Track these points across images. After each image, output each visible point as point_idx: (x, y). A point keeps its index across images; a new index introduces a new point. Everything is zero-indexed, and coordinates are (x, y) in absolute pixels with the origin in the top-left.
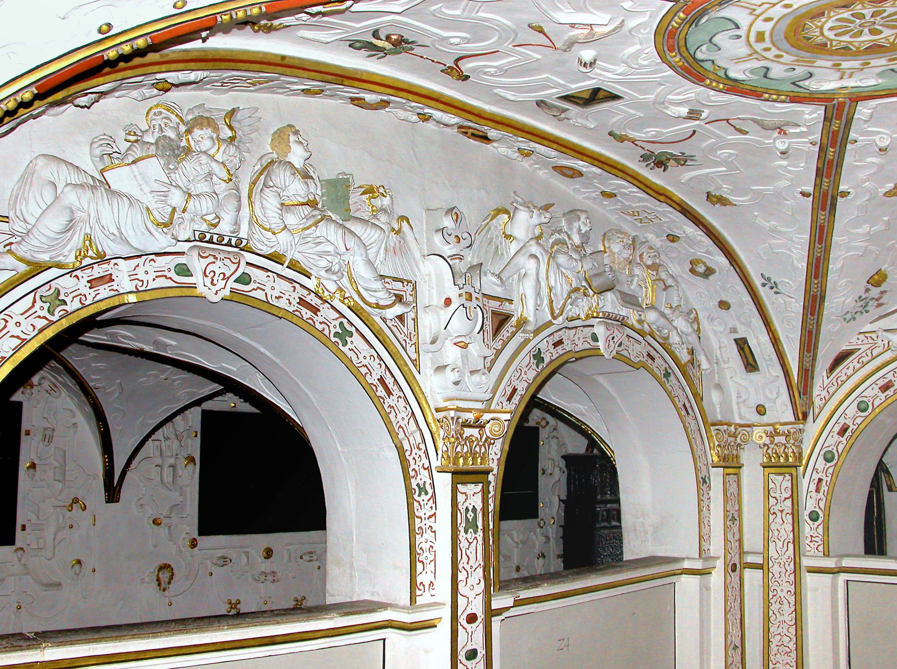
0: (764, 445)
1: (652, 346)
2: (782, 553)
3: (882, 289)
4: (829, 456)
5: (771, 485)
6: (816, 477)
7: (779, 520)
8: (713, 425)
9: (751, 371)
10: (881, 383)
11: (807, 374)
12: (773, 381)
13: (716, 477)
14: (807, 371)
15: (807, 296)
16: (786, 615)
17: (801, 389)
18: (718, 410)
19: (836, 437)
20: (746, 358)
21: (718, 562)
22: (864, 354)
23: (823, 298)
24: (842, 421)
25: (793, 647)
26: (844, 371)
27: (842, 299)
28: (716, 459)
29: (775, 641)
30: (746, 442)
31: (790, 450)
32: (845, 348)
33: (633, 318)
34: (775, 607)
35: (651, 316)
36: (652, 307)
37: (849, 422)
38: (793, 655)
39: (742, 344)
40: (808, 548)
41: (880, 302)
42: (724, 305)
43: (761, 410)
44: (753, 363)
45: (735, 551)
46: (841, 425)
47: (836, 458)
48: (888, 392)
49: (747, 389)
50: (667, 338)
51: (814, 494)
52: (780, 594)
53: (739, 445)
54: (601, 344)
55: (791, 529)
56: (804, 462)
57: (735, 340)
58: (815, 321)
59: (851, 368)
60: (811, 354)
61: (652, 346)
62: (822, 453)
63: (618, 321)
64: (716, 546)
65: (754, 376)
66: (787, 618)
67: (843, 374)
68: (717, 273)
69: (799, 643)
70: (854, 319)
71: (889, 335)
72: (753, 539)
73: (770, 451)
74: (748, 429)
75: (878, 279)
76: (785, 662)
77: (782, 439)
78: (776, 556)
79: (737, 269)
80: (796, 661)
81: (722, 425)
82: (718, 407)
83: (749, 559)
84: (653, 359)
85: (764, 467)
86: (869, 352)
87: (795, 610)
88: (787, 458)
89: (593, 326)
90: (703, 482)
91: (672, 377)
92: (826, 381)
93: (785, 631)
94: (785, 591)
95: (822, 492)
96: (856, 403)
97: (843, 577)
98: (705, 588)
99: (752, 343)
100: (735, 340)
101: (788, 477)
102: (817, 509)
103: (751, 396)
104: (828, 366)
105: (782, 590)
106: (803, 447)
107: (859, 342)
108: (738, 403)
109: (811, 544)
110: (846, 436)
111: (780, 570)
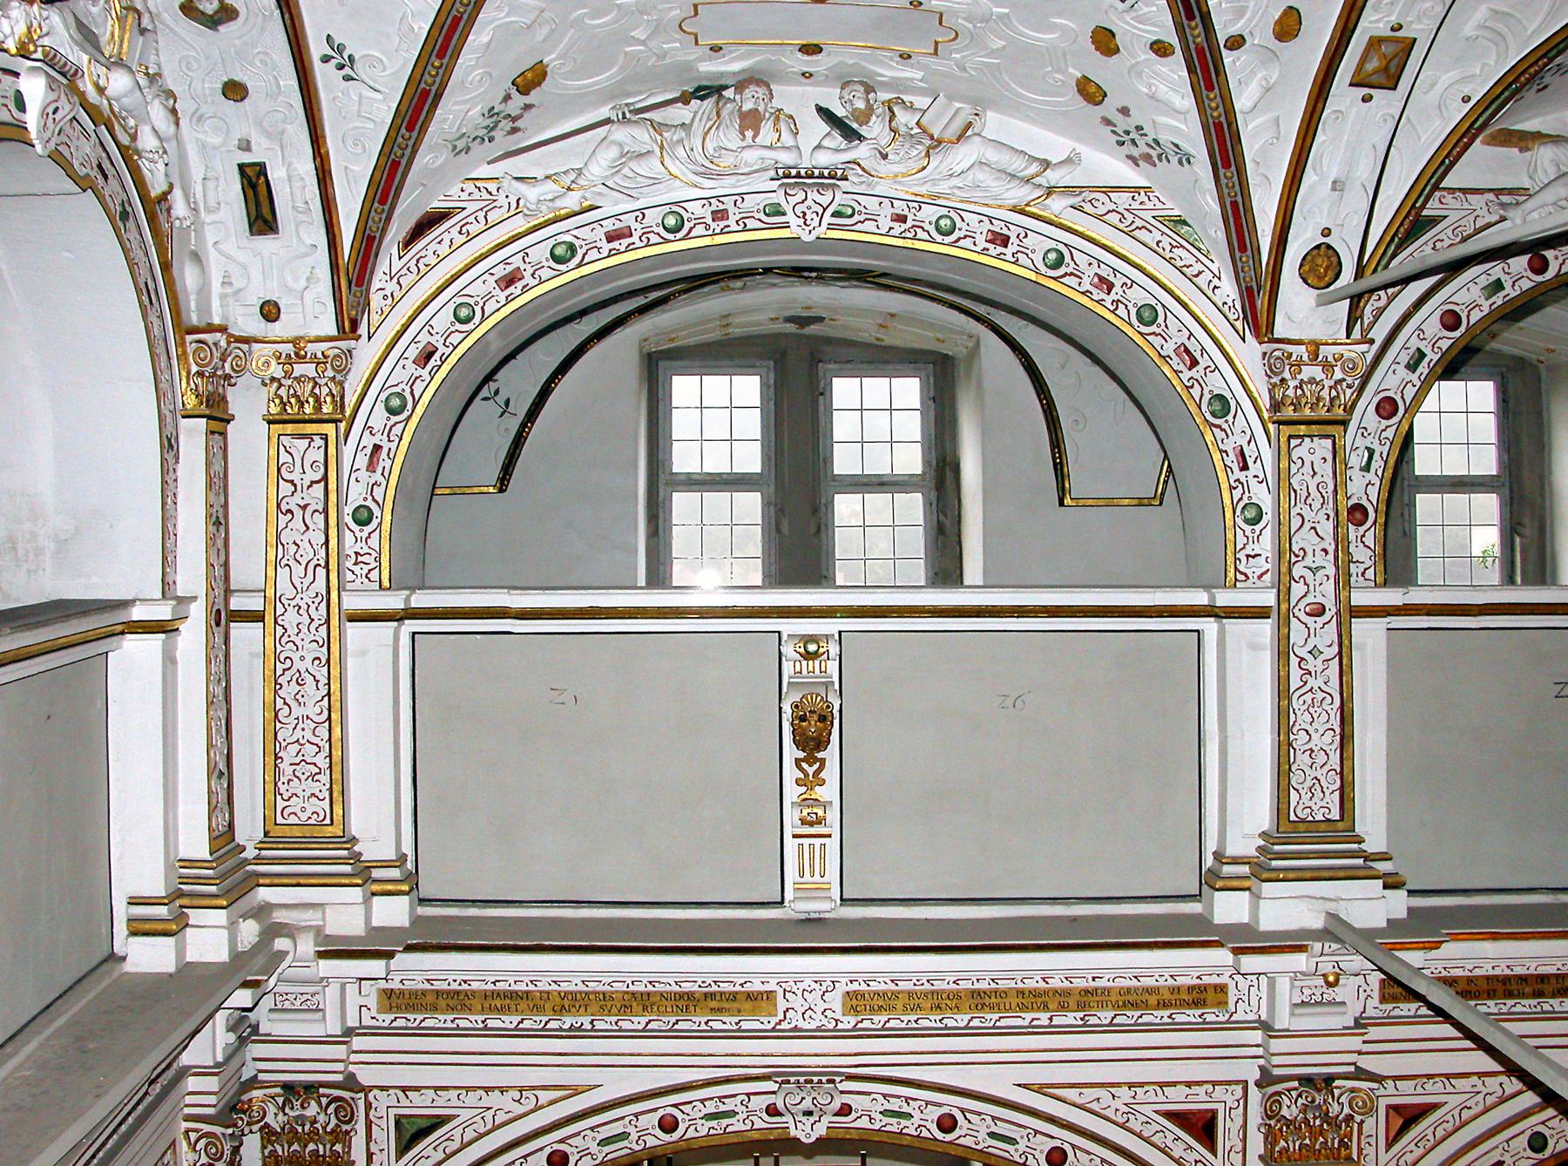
0: (273, 379)
1: (105, 150)
2: (299, 587)
3: (527, 100)
4: (396, 402)
5: (284, 457)
6: (369, 441)
7: (298, 523)
8: (190, 332)
9: (261, 233)
10: (500, 272)
11: (368, 245)
12: (305, 255)
13: (193, 434)
14: (371, 239)
15: (411, 92)
16: (310, 703)
17: (352, 277)
18: (193, 305)
19: (412, 368)
20: (258, 204)
21: (193, 606)
22: (471, 219)
23: (439, 96)
24: (424, 338)
25: (322, 762)
26: (434, 246)
27: (465, 107)
28: (191, 401)
29: (289, 755)
30: (239, 370)
31: (325, 390)
32: (436, 204)
33: (91, 74)
34: (288, 691)
35: (118, 82)
36: (119, 63)
37: (437, 341)
38: (325, 778)
39: (254, 181)
40: (350, 576)
41: (517, 124)
42: (235, 91)
43: (270, 312)
44: (269, 218)
45: (219, 591)
46: (421, 346)
47: (409, 406)
48: (511, 289)
49: (244, 267)
50: (134, 138)
51: (363, 474)
52: (298, 665)
53: (227, 377)
54: (32, 119)
55: (323, 540)
56: (348, 413)
57: (241, 167)
58: (411, 143)
59: (446, 243)
60: (386, 207)
61: (105, 150)
62: (383, 396)
63: (64, 75)
64: (192, 576)
65: (265, 243)
66: (312, 711)
67: (430, 253)
68: (240, 20)
69: (337, 754)
70: (468, 149)
71: (522, 188)
72: (248, 567)
73: (283, 392)
74: (245, 347)
75: (530, 80)
76: (308, 794)
77: (309, 370)
78: (291, 592)
79: (287, 16)
80: (331, 790)
81: (210, 332)
82: (193, 298)
83: (236, 603)
84: (106, 177)
85: (270, 422)
86: (481, 215)
87: (329, 694)
88: (318, 408)
89: (17, 75)
90: (169, 445)
91: (131, 224)
92: (397, 265)
93: (308, 735)
94: (309, 659)
95: (379, 471)
96: (451, 306)
97: (411, 625)
98: (169, 659)
99: (276, 175)
100: (241, 167)
101: (318, 442)
102: (370, 503)
103: (268, 280)
104: (402, 235)
105: (302, 658)
106: (346, 386)
107: (464, 196)
108: (223, 297)
109: (356, 569)
110: (429, 367)
111: (300, 619)
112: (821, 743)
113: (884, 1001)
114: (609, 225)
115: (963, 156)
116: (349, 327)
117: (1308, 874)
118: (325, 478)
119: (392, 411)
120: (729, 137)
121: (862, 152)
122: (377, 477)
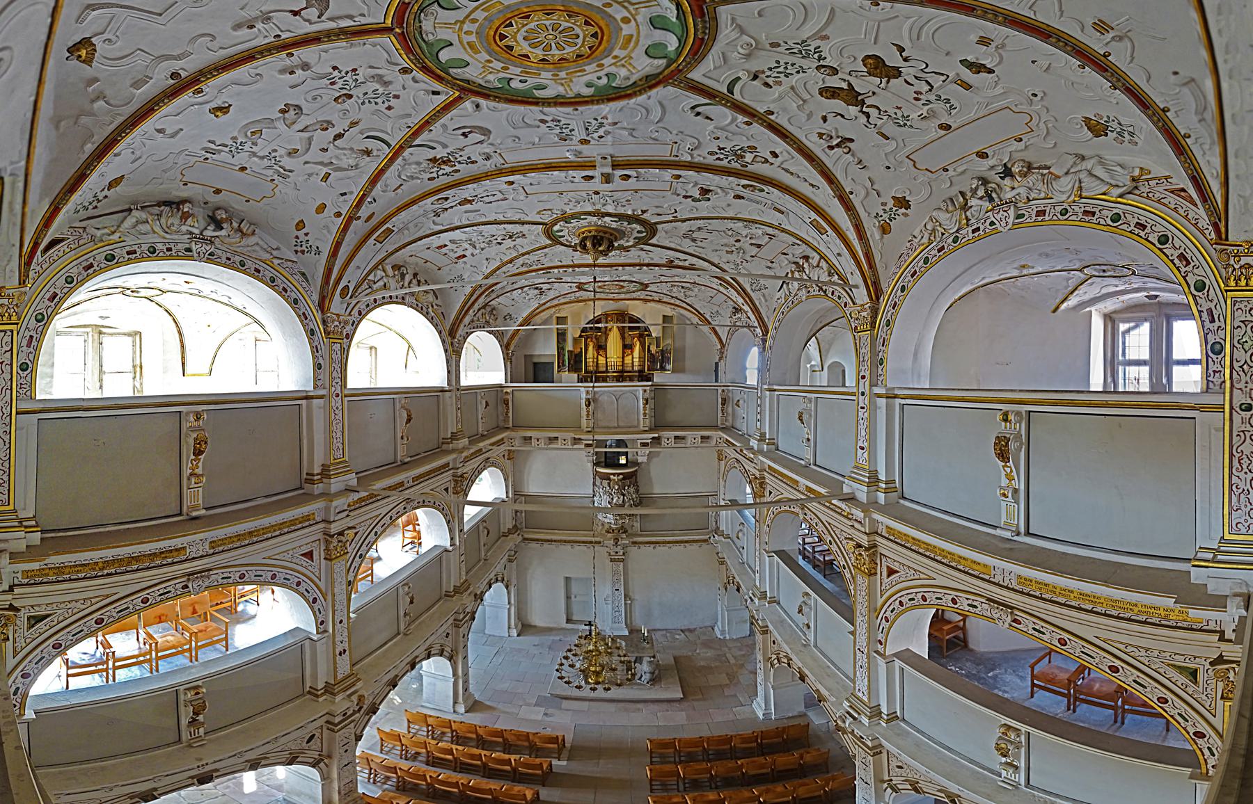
19: (47, 302)
51: (25, 348)
112: (201, 453)
113: (223, 541)
114: (128, 249)
115: (253, 240)
116: (22, 283)
117: (681, 502)
118: (12, 349)
119: (38, 321)
120: (176, 221)
121: (223, 233)
122: (31, 349)
